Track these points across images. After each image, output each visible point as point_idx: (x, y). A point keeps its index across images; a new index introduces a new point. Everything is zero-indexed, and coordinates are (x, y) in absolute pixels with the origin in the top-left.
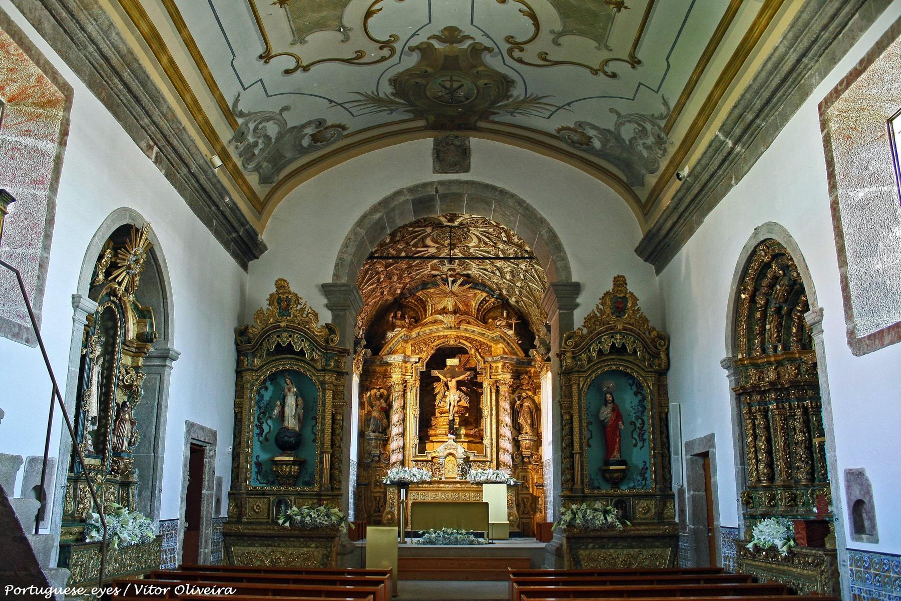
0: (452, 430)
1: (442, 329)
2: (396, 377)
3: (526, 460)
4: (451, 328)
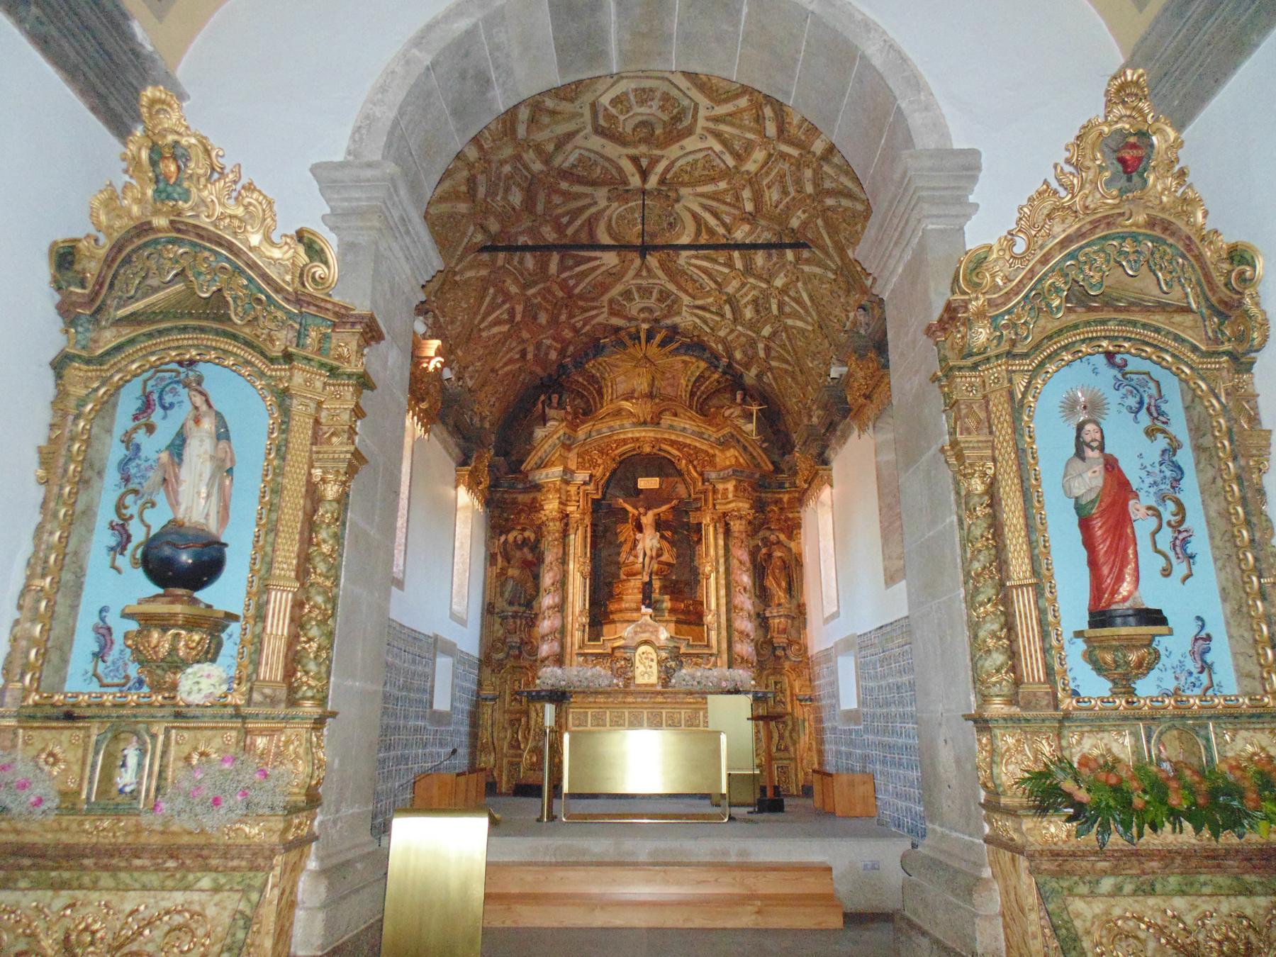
0: (647, 599)
1: (625, 425)
2: (551, 506)
3: (779, 653)
4: (645, 423)
